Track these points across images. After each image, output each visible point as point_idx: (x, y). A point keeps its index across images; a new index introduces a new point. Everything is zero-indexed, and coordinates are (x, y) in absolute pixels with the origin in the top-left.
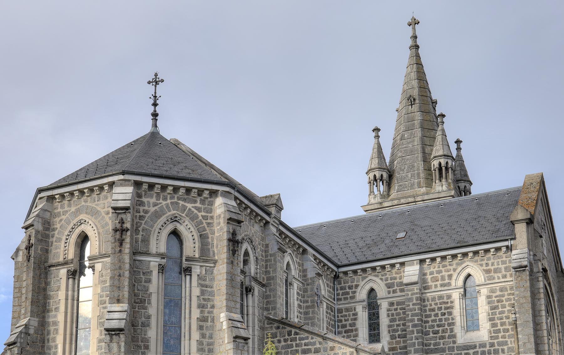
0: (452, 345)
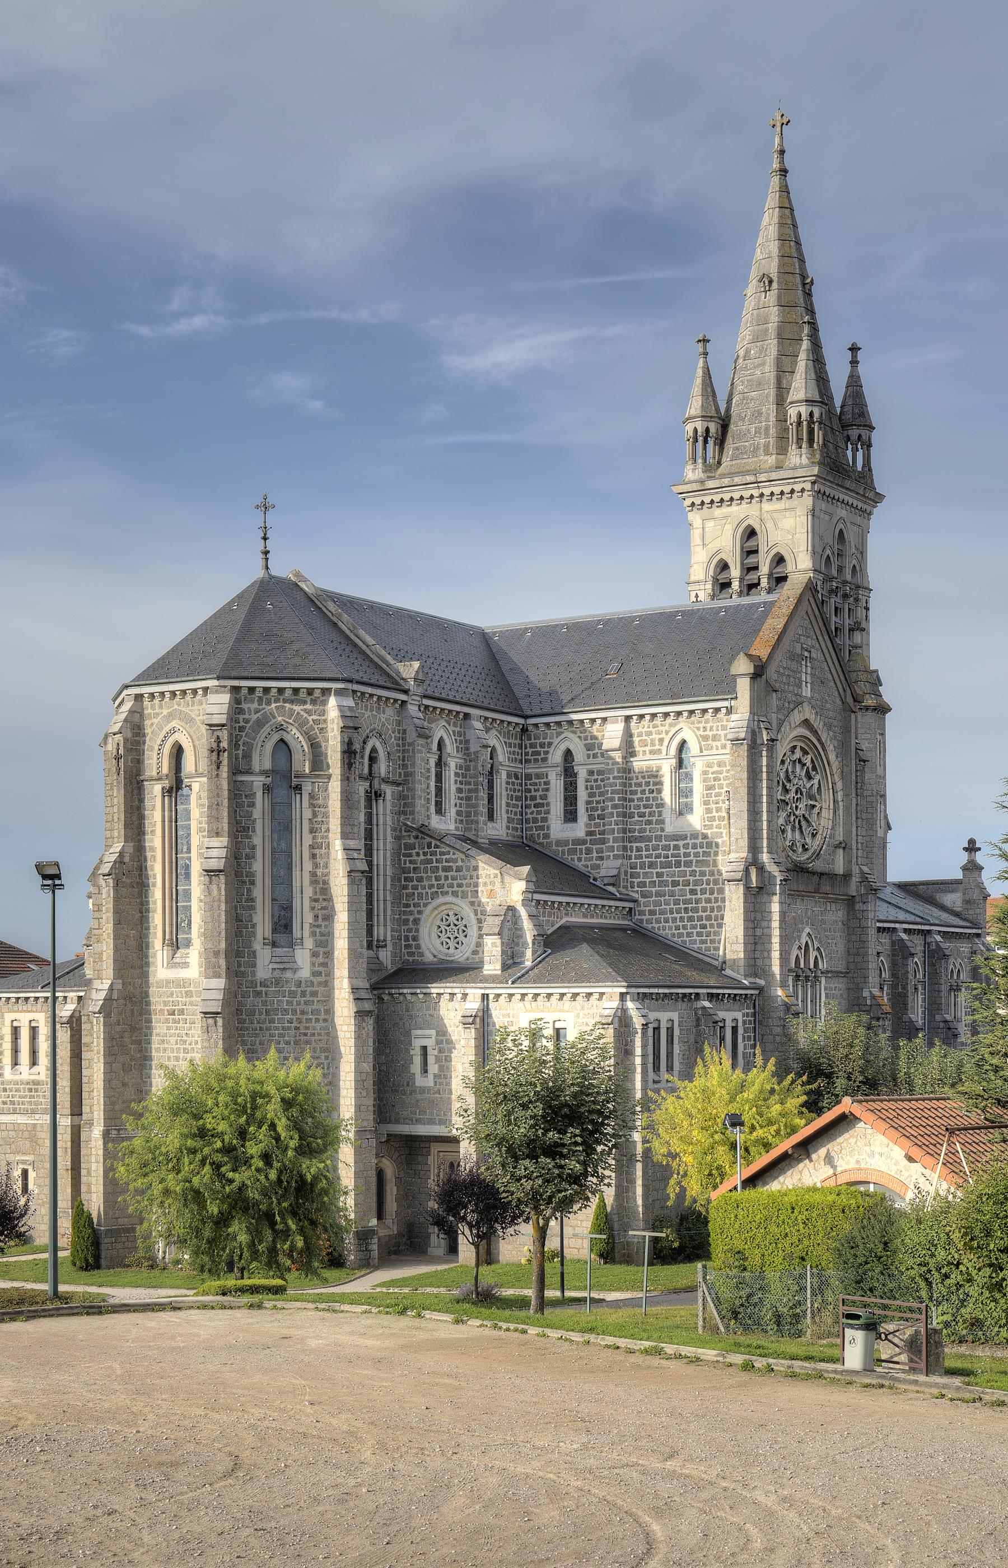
0: (659, 833)
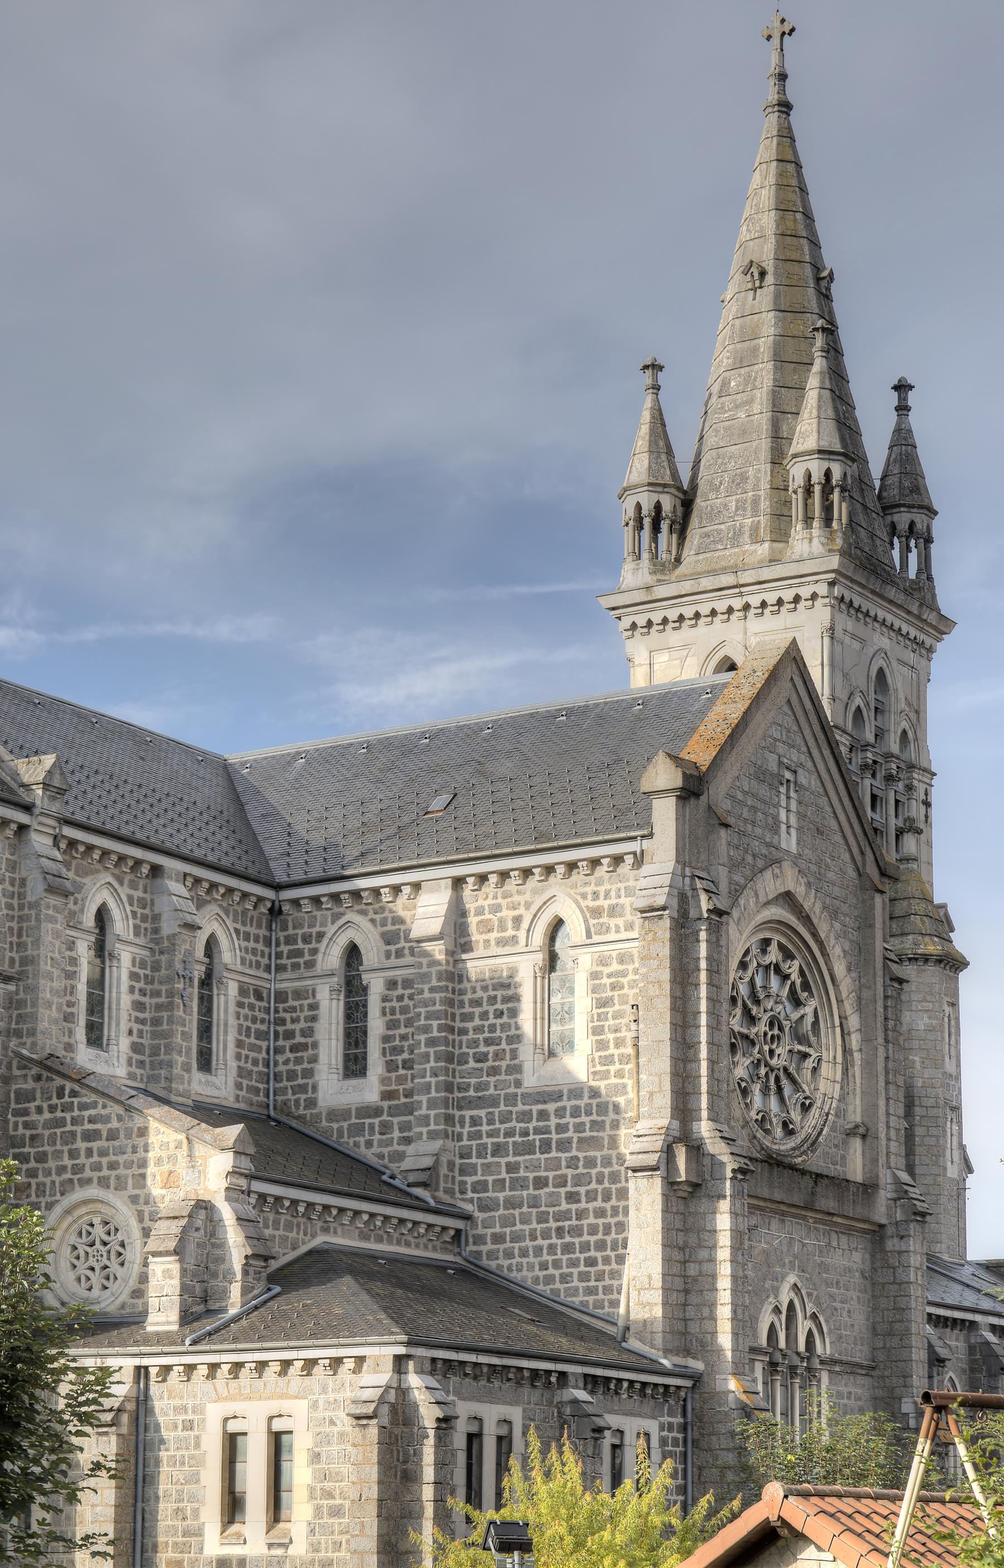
0: (512, 1090)
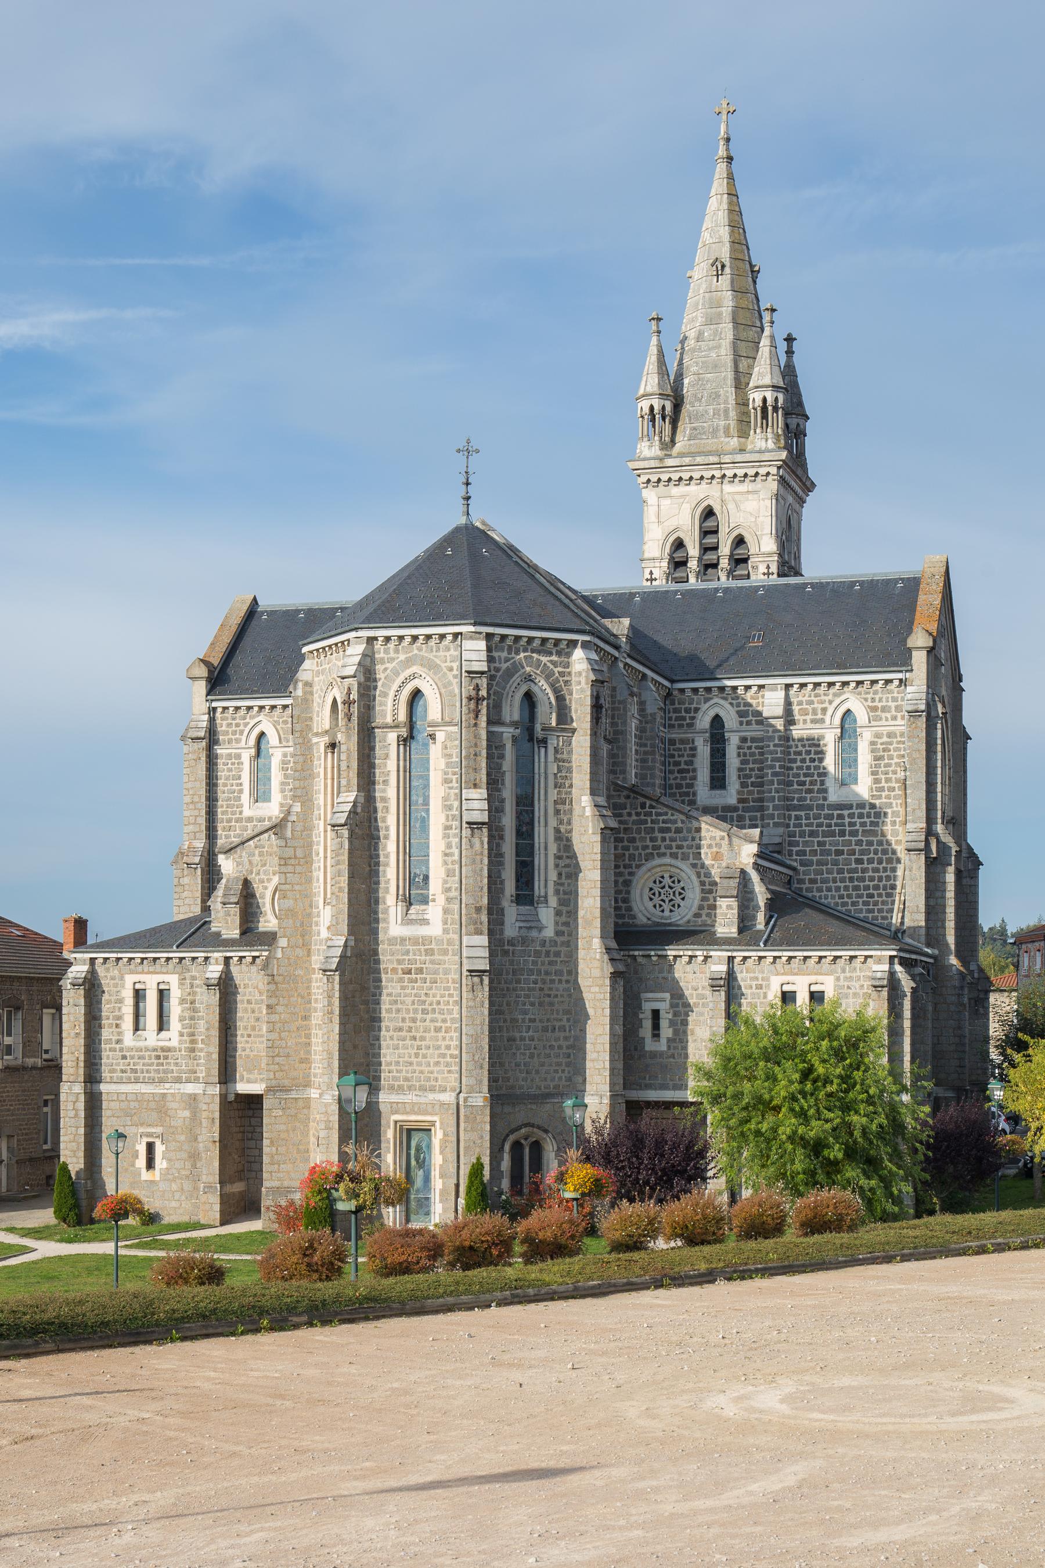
0: (821, 802)
